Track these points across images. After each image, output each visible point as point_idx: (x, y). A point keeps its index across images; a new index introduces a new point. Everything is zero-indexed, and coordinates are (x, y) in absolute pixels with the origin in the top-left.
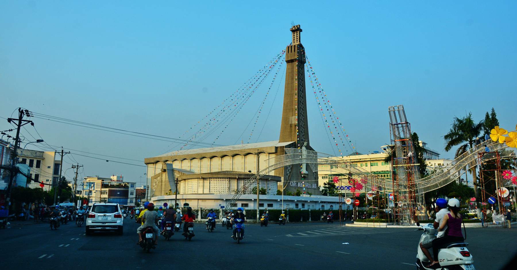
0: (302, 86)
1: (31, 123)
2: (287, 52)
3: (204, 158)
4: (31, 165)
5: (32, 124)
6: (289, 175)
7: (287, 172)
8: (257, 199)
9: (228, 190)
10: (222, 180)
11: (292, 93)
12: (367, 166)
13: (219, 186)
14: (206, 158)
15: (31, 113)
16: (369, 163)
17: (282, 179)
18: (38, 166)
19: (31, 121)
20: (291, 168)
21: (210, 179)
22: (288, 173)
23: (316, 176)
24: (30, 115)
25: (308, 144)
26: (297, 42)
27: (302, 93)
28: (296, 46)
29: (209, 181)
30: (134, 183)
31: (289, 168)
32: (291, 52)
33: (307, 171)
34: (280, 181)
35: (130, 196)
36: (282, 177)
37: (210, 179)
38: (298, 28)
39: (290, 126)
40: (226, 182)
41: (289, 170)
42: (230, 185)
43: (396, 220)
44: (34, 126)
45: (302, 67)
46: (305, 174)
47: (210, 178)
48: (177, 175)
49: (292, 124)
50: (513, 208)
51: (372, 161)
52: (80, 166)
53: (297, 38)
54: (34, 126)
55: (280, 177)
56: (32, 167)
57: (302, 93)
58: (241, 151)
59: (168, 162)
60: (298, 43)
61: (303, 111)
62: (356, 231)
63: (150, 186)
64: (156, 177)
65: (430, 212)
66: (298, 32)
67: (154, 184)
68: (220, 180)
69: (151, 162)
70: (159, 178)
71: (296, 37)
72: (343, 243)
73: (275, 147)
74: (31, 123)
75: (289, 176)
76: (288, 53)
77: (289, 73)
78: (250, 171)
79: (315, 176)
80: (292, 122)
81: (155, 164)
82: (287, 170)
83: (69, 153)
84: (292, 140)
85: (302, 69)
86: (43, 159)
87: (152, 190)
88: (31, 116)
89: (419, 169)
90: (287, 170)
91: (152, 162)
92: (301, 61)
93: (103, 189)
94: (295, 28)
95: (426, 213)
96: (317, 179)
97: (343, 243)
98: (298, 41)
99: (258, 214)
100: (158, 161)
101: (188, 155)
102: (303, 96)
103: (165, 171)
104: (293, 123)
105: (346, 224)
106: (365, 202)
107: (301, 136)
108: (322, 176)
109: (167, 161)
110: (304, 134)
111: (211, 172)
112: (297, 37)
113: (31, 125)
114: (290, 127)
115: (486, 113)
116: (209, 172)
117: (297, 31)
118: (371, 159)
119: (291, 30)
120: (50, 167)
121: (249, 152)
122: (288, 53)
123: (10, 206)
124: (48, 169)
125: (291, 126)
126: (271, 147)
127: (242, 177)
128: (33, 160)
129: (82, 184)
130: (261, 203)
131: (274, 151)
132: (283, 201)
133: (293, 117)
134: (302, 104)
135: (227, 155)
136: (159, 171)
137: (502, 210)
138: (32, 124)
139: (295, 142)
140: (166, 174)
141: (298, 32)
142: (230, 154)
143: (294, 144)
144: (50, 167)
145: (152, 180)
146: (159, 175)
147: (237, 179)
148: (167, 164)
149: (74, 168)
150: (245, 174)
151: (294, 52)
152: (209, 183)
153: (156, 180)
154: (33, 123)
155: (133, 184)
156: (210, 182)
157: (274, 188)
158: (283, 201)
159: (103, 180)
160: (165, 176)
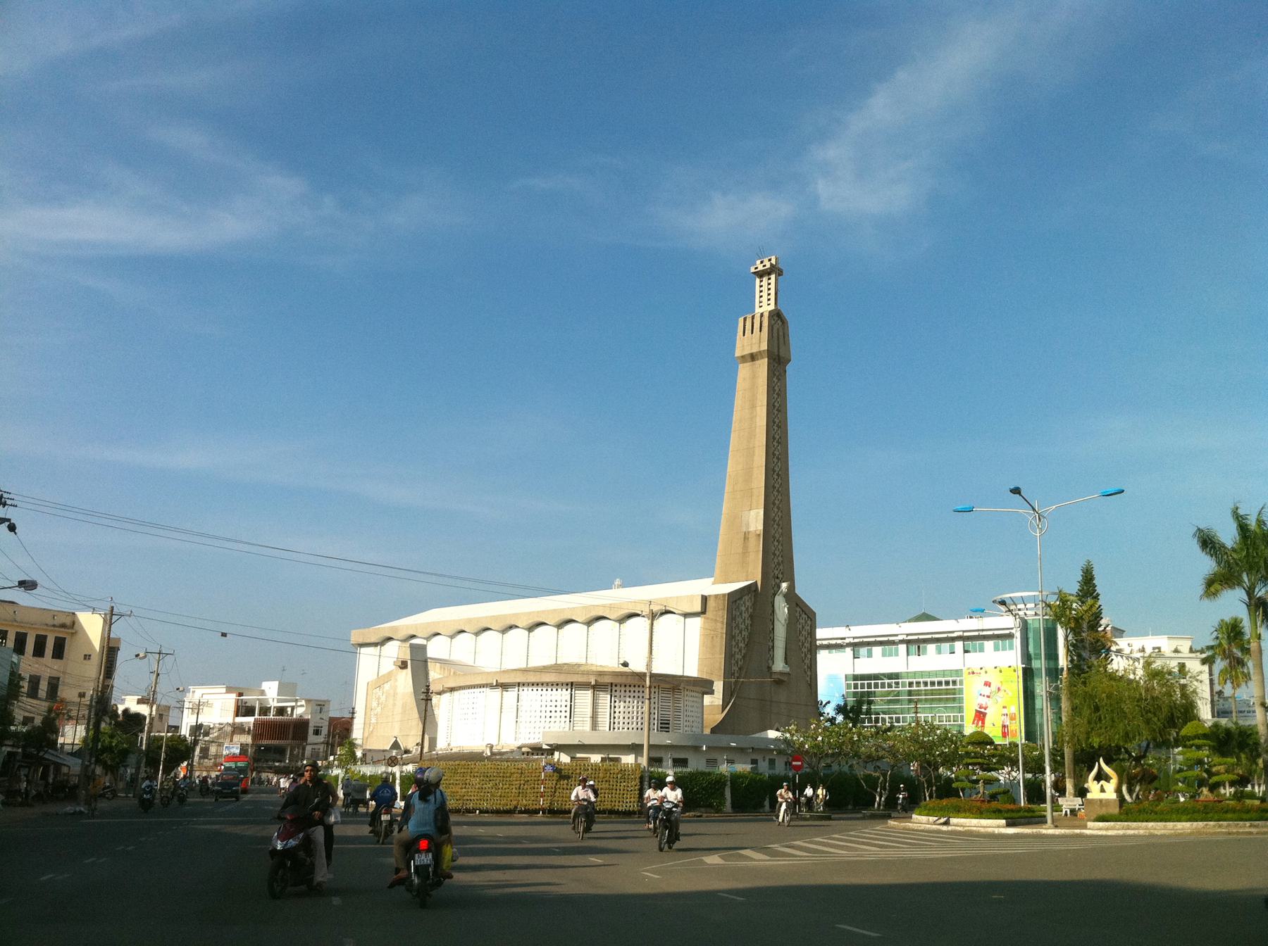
0: (779, 427)
1: (7, 523)
3: (511, 627)
4: (39, 651)
5: (12, 528)
7: (734, 668)
8: (642, 746)
11: (751, 446)
12: (954, 653)
14: (517, 627)
15: (10, 496)
16: (959, 645)
17: (718, 686)
18: (59, 652)
19: (9, 520)
20: (744, 657)
21: (519, 686)
23: (811, 678)
24: (9, 502)
25: (792, 587)
26: (769, 305)
27: (777, 446)
28: (766, 315)
29: (516, 693)
30: (324, 701)
31: (737, 656)
33: (786, 664)
34: (712, 692)
35: (312, 738)
36: (719, 680)
37: (519, 686)
38: (771, 264)
39: (743, 537)
41: (737, 662)
42: (573, 704)
43: (874, 688)
44: (15, 533)
45: (780, 374)
46: (781, 673)
47: (519, 684)
48: (435, 674)
49: (749, 532)
51: (969, 638)
52: (167, 654)
53: (769, 300)
54: (15, 533)
55: (712, 683)
57: (777, 446)
58: (610, 607)
59: (414, 641)
60: (772, 307)
61: (779, 497)
62: (915, 844)
64: (380, 682)
65: (1130, 791)
66: (773, 277)
67: (374, 704)
69: (368, 641)
70: (387, 686)
73: (702, 596)
74: (7, 523)
76: (744, 335)
77: (745, 390)
78: (625, 664)
79: (808, 679)
80: (748, 525)
81: (379, 647)
83: (130, 616)
84: (747, 576)
85: (779, 380)
86: (72, 633)
87: (367, 722)
88: (11, 505)
90: (733, 662)
91: (373, 640)
92: (778, 356)
93: (240, 720)
94: (764, 266)
95: (1118, 791)
98: (772, 302)
100: (390, 639)
101: (469, 621)
102: (780, 422)
103: (403, 665)
104: (752, 529)
105: (889, 821)
107: (773, 566)
109: (413, 636)
110: (780, 559)
112: (769, 289)
113: (7, 529)
114: (744, 540)
115: (1083, 563)
116: (523, 666)
117: (769, 274)
118: (966, 634)
120: (90, 656)
121: (633, 611)
125: (746, 537)
126: (691, 598)
127: (607, 680)
129: (180, 706)
130: (655, 754)
131: (698, 608)
133: (753, 513)
134: (776, 477)
135: (574, 619)
136: (388, 665)
137: (1057, 688)
138: (12, 528)
139: (756, 582)
140: (407, 674)
141: (773, 277)
142: (553, 620)
143: (753, 589)
144: (90, 656)
145: (370, 692)
146: (389, 677)
147: (594, 686)
148: (412, 646)
149: (140, 659)
150: (614, 672)
153: (378, 692)
154: (14, 525)
159: (240, 694)
160: (405, 678)
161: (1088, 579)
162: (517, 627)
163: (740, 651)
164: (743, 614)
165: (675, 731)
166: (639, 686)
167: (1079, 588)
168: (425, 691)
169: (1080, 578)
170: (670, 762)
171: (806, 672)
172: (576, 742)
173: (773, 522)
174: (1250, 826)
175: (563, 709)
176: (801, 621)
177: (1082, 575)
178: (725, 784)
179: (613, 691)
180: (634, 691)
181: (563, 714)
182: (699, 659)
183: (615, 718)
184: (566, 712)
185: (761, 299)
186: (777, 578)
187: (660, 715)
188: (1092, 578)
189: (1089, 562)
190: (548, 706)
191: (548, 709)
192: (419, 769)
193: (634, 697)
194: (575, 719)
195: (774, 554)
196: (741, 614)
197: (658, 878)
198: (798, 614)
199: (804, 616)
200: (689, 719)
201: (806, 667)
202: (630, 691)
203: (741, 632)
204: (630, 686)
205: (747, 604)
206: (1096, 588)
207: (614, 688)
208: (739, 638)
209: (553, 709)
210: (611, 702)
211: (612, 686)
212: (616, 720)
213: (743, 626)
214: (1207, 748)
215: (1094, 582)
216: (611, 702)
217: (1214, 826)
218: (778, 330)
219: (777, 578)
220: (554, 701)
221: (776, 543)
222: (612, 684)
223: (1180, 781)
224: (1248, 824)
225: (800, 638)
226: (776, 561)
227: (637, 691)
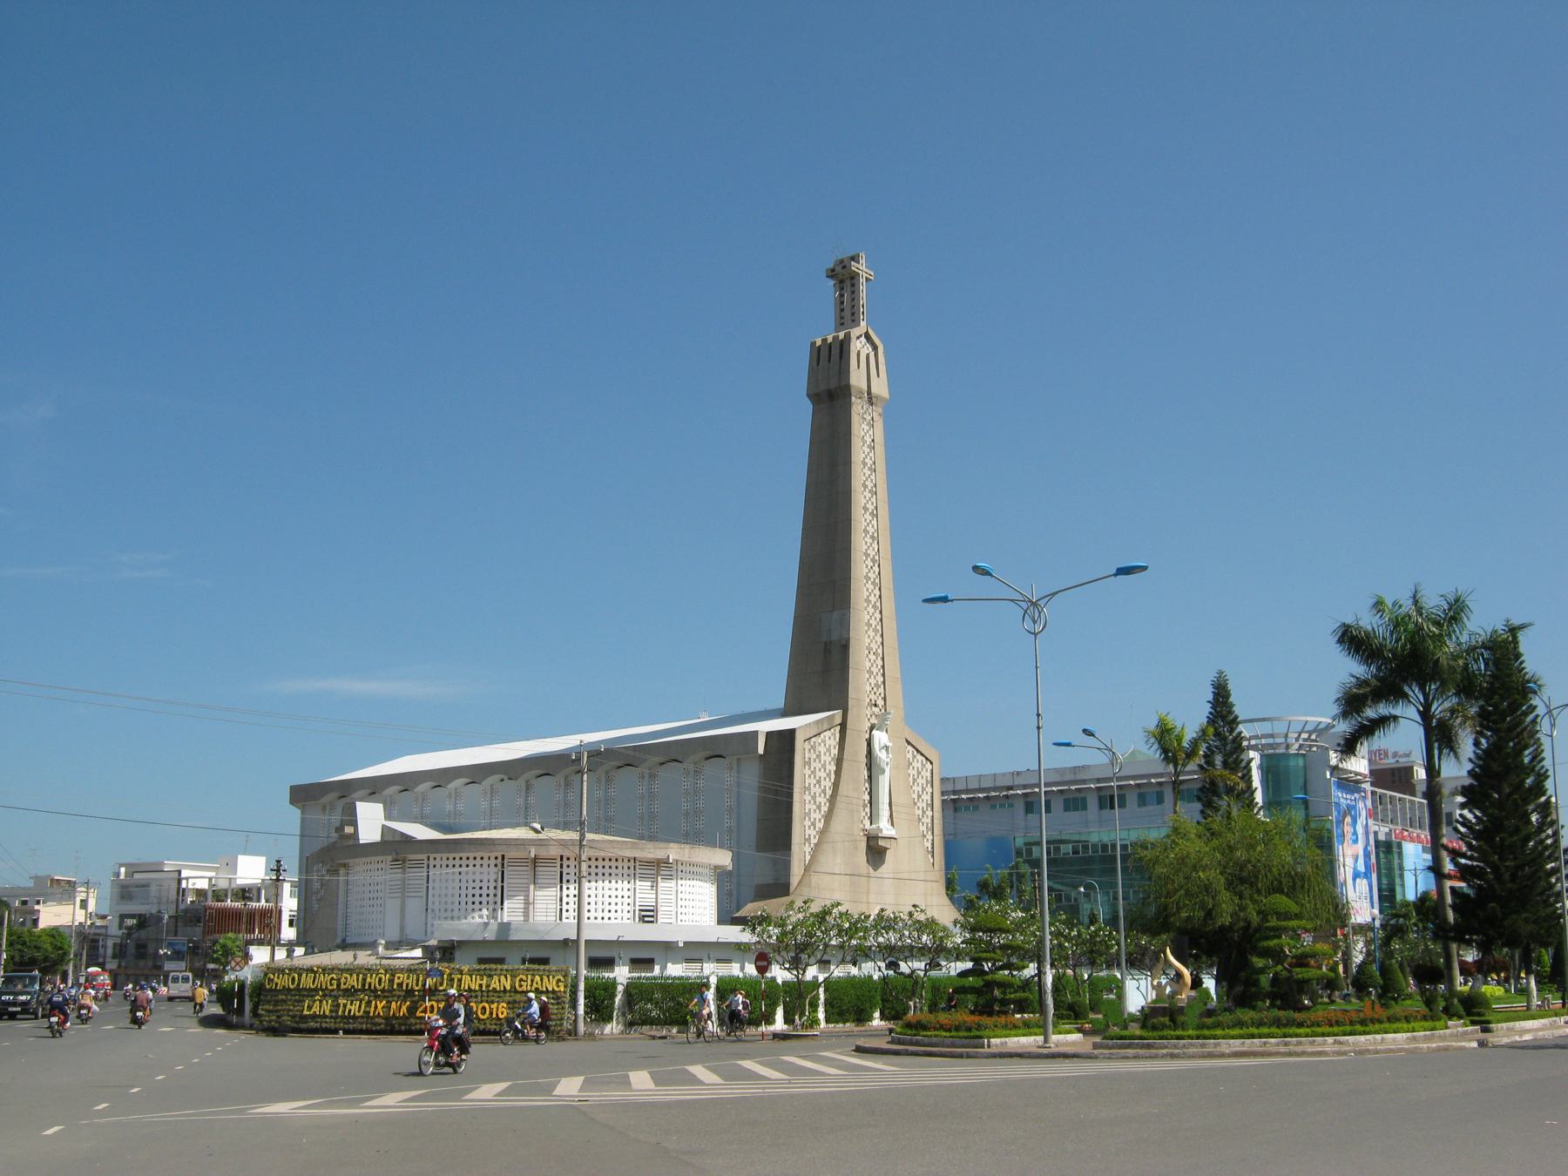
2: (815, 363)
6: (814, 841)
7: (808, 832)
10: (568, 866)
13: (600, 899)
22: (812, 832)
31: (813, 815)
32: (827, 359)
40: (474, 873)
41: (813, 824)
49: (831, 642)
50: (169, 953)
56: (291, 787)
68: (568, 866)
71: (849, 308)
75: (816, 845)
76: (818, 364)
89: (1541, 827)
106: (70, 955)
107: (869, 689)
115: (1211, 676)
119: (830, 274)
122: (818, 364)
124: (1067, 813)
151: (826, 362)
152: (426, 880)
157: (691, 897)
161: (1221, 696)
163: (819, 807)
165: (646, 919)
169: (1210, 697)
171: (924, 836)
172: (714, 939)
173: (866, 628)
174: (1335, 1042)
177: (1213, 692)
178: (707, 986)
179: (565, 867)
182: (758, 820)
184: (568, 896)
186: (875, 705)
187: (637, 900)
188: (1227, 695)
189: (1221, 673)
191: (471, 892)
193: (597, 874)
197: (138, 1091)
200: (687, 903)
203: (819, 782)
205: (828, 742)
206: (1234, 709)
207: (565, 863)
210: (502, 887)
211: (562, 860)
213: (823, 775)
214: (282, 942)
216: (502, 887)
217: (1277, 1045)
218: (868, 356)
219: (875, 705)
221: (872, 657)
224: (1330, 1040)
226: (872, 681)
227: (614, 867)
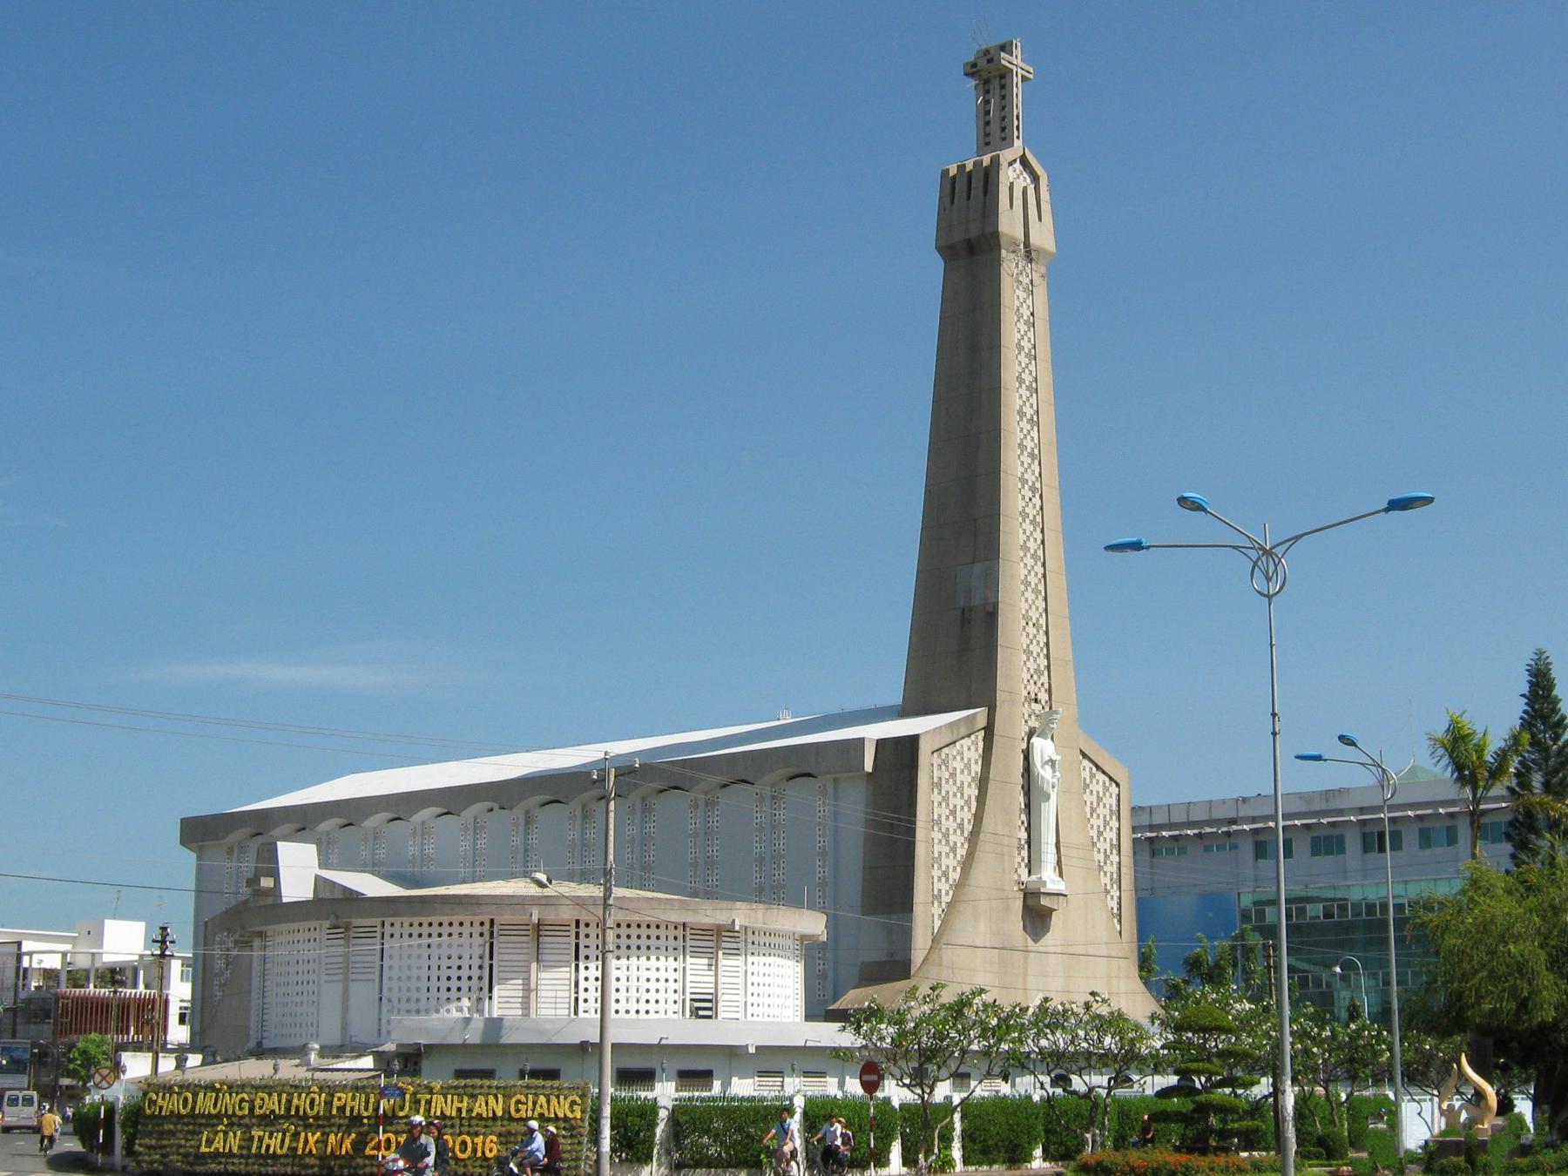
6: (946, 899)
7: (937, 886)
9: (384, 1022)
22: (944, 886)
41: (945, 874)
63: (556, 1083)
72: (101, 1131)
75: (949, 904)
82: (936, 873)
96: (200, 960)
97: (101, 1131)
99: (118, 1123)
108: (673, 925)
111: (1190, 820)
115: (1527, 657)
123: (869, 774)
128: (613, 1045)
132: (1368, 936)
155: (526, 964)
156: (577, 945)
158: (1368, 936)
162: (1356, 746)
163: (954, 850)
164: (959, 777)
166: (629, 926)
167: (1526, 708)
168: (159, 938)
169: (1525, 689)
170: (454, 1010)
173: (1023, 588)
175: (622, 985)
176: (1094, 787)
180: (648, 937)
181: (622, 995)
182: (864, 868)
183: (481, 967)
184: (586, 979)
185: (988, 128)
189: (1540, 653)
190: (443, 968)
192: (43, 999)
194: (567, 994)
195: (1028, 652)
196: (953, 775)
198: (1086, 774)
199: (1100, 776)
201: (1108, 880)
202: (629, 937)
204: (629, 926)
205: (966, 755)
208: (951, 824)
209: (454, 973)
212: (475, 973)
215: (1554, 693)
220: (455, 957)
221: (1031, 630)
222: (684, 924)
223: (1439, 1045)
225: (1094, 821)
226: (1032, 665)
227: (653, 937)
